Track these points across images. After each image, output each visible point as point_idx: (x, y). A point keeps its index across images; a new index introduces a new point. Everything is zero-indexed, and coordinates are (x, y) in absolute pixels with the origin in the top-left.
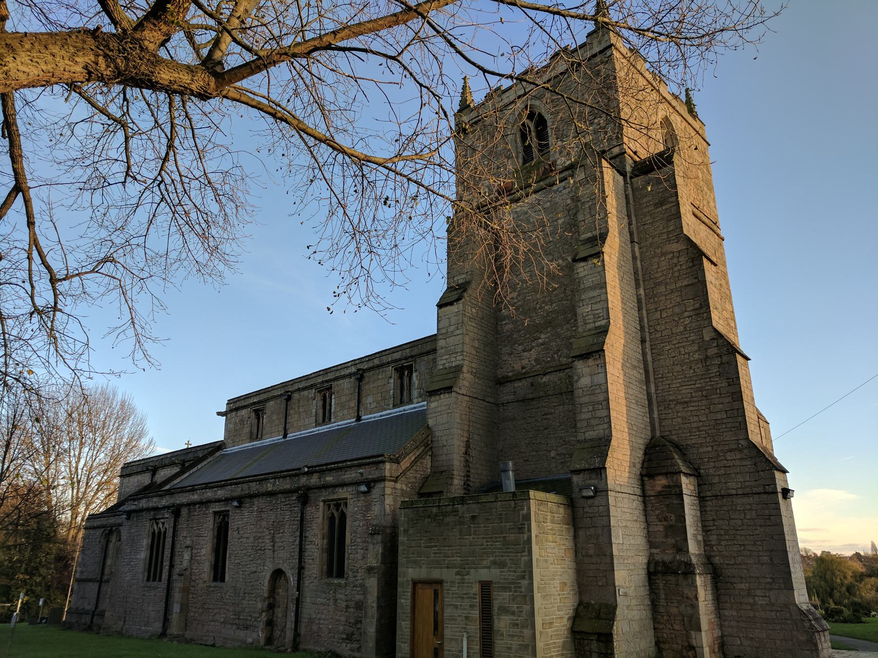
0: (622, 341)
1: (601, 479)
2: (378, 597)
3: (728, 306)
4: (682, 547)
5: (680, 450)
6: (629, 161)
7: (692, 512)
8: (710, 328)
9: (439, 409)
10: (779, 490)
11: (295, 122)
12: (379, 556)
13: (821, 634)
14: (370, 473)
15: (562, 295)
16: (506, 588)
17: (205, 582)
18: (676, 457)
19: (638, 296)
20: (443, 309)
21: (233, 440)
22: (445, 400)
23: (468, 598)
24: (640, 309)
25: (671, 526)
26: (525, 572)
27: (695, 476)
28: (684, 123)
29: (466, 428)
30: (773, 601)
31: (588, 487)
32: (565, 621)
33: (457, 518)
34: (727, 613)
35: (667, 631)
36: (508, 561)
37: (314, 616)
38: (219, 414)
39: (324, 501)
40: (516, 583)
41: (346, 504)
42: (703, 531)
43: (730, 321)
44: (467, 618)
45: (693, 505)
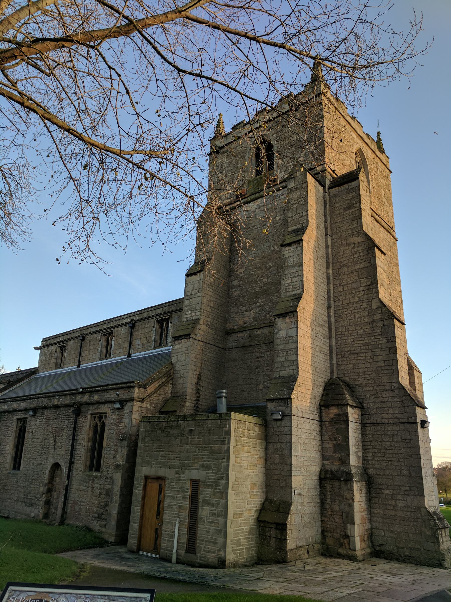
0: (312, 306)
1: (288, 407)
2: (121, 488)
4: (345, 461)
5: (350, 388)
6: (328, 177)
8: (377, 300)
9: (180, 350)
10: (419, 421)
11: (41, 112)
12: (125, 456)
13: (443, 530)
14: (123, 394)
15: (276, 272)
16: (209, 485)
17: (7, 470)
18: (346, 393)
20: (190, 278)
21: (43, 367)
24: (328, 284)
25: (339, 444)
26: (223, 474)
27: (360, 408)
28: (374, 155)
29: (199, 365)
30: (409, 504)
31: (277, 412)
33: (180, 430)
34: (376, 511)
35: (330, 523)
36: (213, 466)
37: (77, 499)
38: (36, 348)
39: (92, 414)
40: (216, 482)
41: (106, 416)
42: (363, 449)
44: (180, 507)
45: (357, 429)
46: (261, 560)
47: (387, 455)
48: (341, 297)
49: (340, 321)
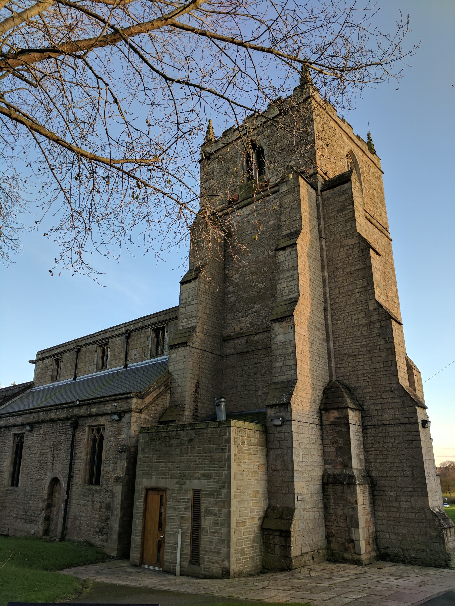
0: (309, 310)
1: (288, 412)
2: (122, 501)
3: (393, 287)
4: (347, 464)
5: (350, 391)
7: (357, 438)
8: (373, 301)
9: (177, 359)
10: (420, 421)
11: (29, 123)
12: (125, 469)
13: (448, 530)
15: (270, 276)
16: (211, 494)
17: (5, 486)
18: (346, 395)
19: (323, 277)
21: (39, 381)
22: (182, 351)
23: (184, 502)
24: (324, 287)
26: (225, 483)
27: (360, 410)
28: (365, 156)
29: (197, 373)
30: (413, 505)
31: (277, 418)
32: (256, 520)
34: (380, 514)
35: (334, 528)
37: (77, 514)
38: (31, 362)
39: (89, 427)
40: (218, 491)
42: (365, 452)
43: (394, 298)
44: (182, 518)
46: (266, 569)
47: (389, 456)
48: (337, 300)
49: (337, 324)
